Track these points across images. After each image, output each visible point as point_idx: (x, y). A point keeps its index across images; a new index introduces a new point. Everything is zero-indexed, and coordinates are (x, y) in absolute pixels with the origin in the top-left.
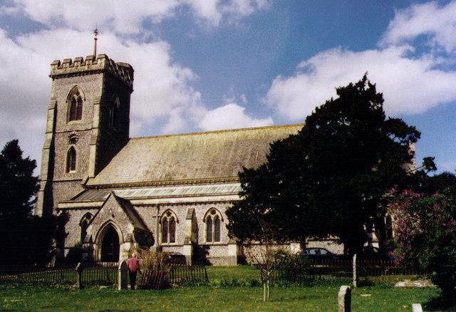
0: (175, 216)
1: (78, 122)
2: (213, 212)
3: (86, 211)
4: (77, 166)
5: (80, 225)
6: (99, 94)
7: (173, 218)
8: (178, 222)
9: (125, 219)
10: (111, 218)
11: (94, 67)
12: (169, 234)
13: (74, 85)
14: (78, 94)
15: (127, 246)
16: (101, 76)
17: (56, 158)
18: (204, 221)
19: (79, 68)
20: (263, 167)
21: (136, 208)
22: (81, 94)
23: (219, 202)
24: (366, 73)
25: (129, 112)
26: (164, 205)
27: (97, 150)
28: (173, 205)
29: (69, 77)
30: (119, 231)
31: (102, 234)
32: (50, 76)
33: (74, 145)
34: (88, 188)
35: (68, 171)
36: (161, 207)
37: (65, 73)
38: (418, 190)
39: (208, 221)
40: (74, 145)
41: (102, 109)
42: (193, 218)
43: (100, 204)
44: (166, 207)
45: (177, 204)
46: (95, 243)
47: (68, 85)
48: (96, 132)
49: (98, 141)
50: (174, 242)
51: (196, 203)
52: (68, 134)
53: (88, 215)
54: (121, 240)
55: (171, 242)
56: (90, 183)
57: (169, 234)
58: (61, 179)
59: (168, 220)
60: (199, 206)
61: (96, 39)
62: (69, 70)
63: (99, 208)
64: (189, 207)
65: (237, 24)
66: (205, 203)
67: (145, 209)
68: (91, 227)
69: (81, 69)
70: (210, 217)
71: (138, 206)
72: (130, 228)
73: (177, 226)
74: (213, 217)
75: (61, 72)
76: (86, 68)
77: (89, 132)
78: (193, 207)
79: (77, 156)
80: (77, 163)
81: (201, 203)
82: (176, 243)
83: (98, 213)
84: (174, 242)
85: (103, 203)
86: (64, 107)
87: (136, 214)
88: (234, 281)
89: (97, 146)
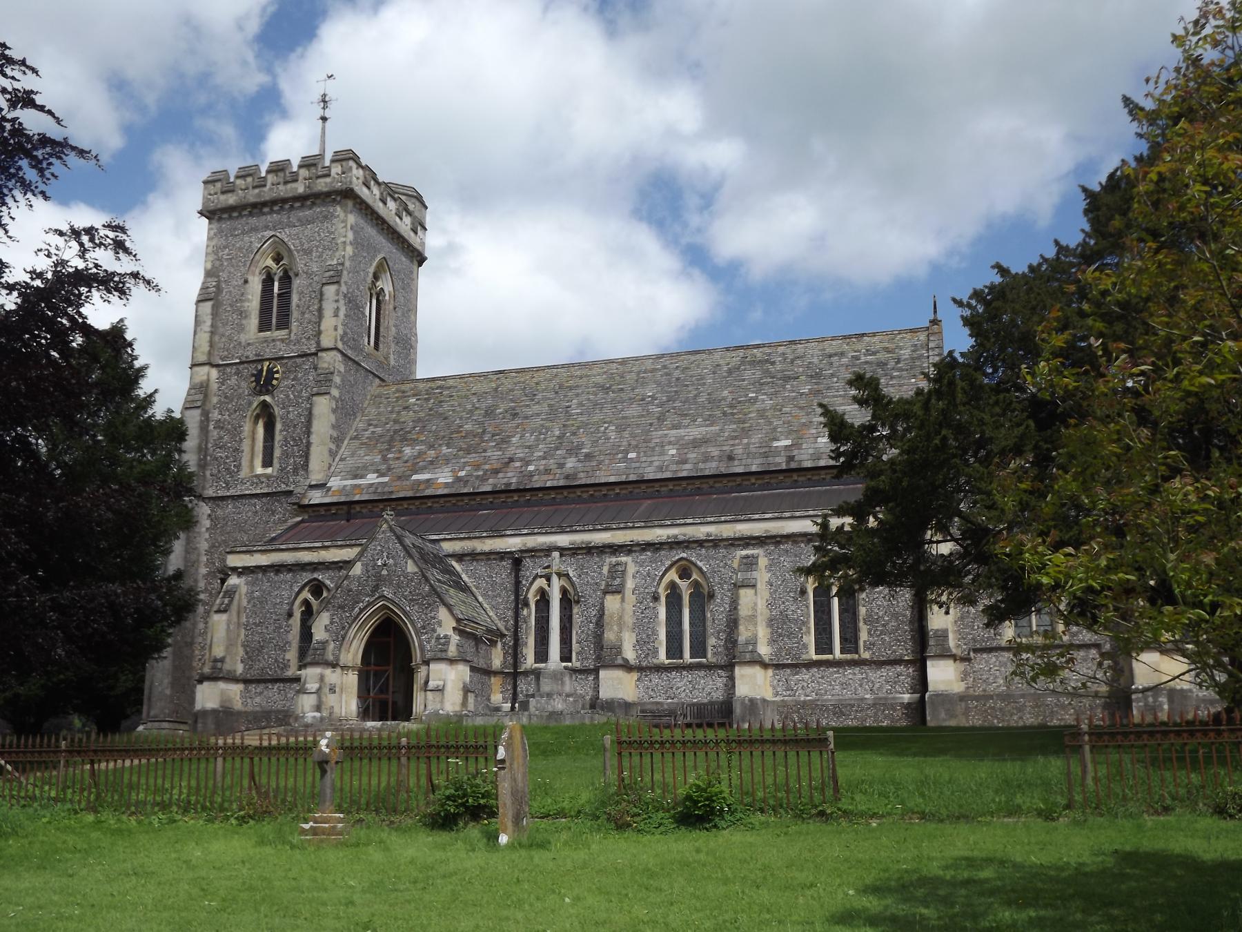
1: (282, 333)
4: (275, 461)
17: (1041, 759)
20: (852, 425)
23: (700, 543)
24: (954, 300)
32: (201, 213)
33: (268, 398)
36: (528, 562)
40: (268, 398)
47: (257, 240)
52: (252, 369)
53: (317, 589)
54: (417, 656)
58: (232, 492)
61: (324, 119)
62: (252, 196)
65: (607, 462)
69: (284, 191)
71: (460, 557)
75: (231, 200)
76: (300, 188)
80: (277, 445)
84: (569, 660)
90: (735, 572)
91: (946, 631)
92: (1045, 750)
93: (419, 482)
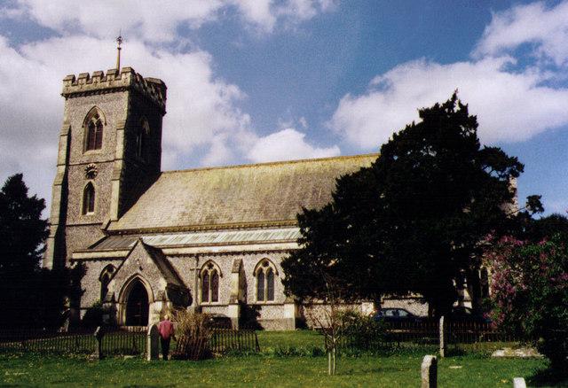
0: (217, 269)
1: (97, 151)
2: (266, 264)
3: (107, 263)
5: (100, 279)
6: (124, 117)
7: (216, 271)
8: (221, 276)
9: (156, 273)
10: (139, 271)
11: (117, 84)
12: (210, 291)
13: (93, 105)
14: (97, 116)
15: (158, 306)
16: (125, 95)
17: (69, 196)
18: (254, 275)
19: (99, 84)
21: (170, 259)
22: (101, 117)
24: (456, 91)
25: (160, 139)
26: (204, 255)
27: (121, 187)
28: (215, 254)
29: (85, 96)
30: (148, 287)
31: (127, 290)
32: (62, 95)
33: (92, 181)
34: (109, 234)
35: (84, 213)
36: (200, 258)
37: (81, 90)
38: (520, 236)
39: (259, 275)
40: (92, 181)
41: (127, 136)
42: (241, 271)
43: (124, 253)
44: (207, 258)
45: (221, 254)
46: (118, 302)
47: (85, 106)
48: (119, 164)
49: (122, 176)
50: (217, 300)
51: (244, 253)
52: (85, 167)
53: (110, 268)
55: (213, 301)
56: (112, 227)
57: (210, 291)
58: (76, 223)
59: (209, 274)
60: (247, 256)
61: (119, 49)
62: (86, 87)
63: (124, 259)
64: (236, 257)
66: (256, 252)
67: (181, 260)
68: (113, 282)
69: (101, 85)
70: (261, 270)
71: (172, 256)
72: (162, 284)
73: (221, 281)
74: (265, 270)
75: (76, 89)
76: (107, 85)
77: (110, 165)
78: (241, 257)
79: (96, 194)
80: (96, 202)
81: (250, 253)
82: (219, 302)
83: (122, 265)
84: (217, 300)
85: (128, 252)
86: (79, 133)
87: (169, 266)
88: (291, 350)
89: (121, 181)
90: (439, 357)
91: (542, 210)
92: (61, 211)
93: (459, 365)
